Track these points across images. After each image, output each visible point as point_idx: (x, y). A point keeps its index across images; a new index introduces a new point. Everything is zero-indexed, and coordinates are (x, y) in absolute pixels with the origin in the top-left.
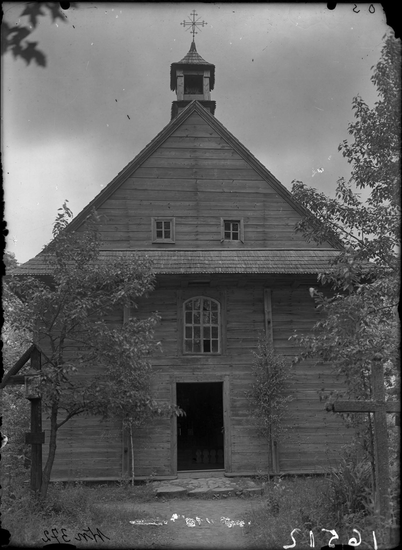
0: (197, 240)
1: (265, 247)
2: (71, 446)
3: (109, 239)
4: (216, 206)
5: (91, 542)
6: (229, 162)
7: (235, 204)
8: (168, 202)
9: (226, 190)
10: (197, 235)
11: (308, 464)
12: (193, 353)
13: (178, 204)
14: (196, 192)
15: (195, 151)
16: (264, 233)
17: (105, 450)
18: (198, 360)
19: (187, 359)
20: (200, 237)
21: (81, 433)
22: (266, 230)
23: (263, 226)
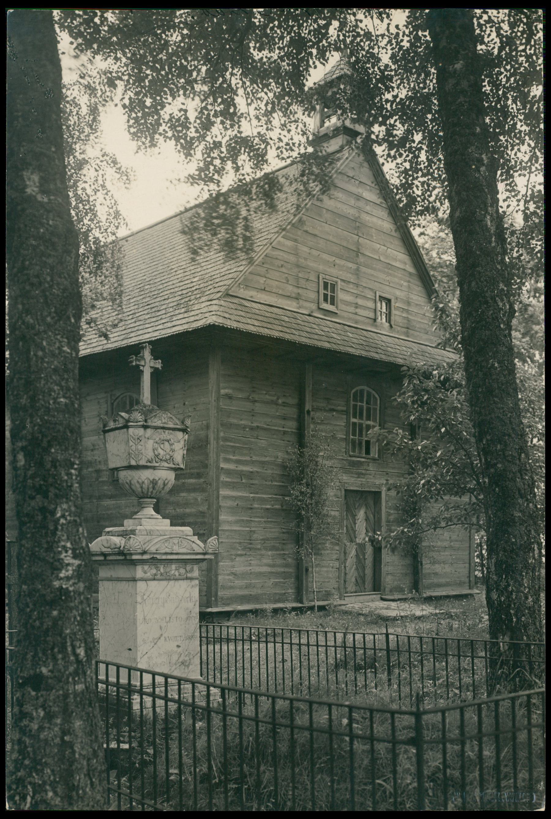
0: (356, 314)
1: (408, 336)
2: (250, 565)
3: (280, 292)
4: (372, 275)
5: (15, 460)
6: (380, 222)
7: (388, 278)
8: (334, 258)
9: (382, 259)
10: (356, 307)
11: (439, 585)
12: (357, 454)
13: (342, 262)
14: (358, 253)
15: (358, 200)
16: (408, 320)
17: (282, 570)
18: (361, 463)
19: (353, 461)
20: (359, 311)
21: (259, 547)
22: (410, 317)
23: (407, 311)
